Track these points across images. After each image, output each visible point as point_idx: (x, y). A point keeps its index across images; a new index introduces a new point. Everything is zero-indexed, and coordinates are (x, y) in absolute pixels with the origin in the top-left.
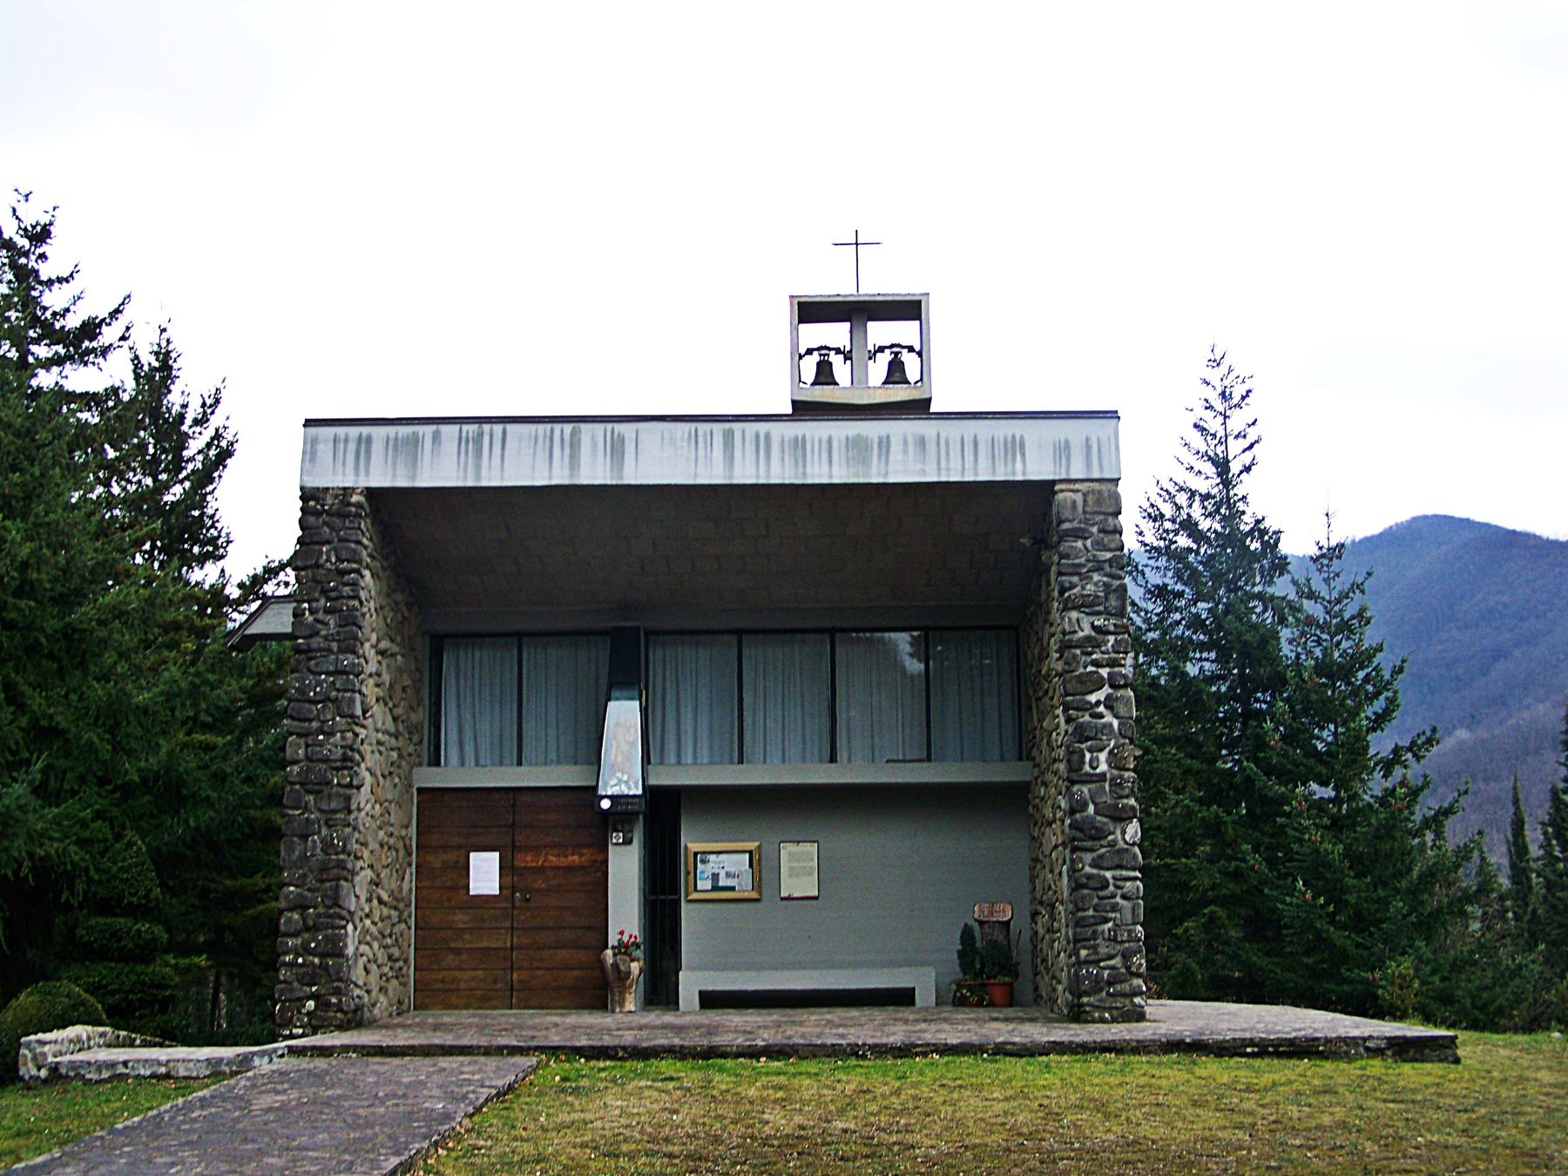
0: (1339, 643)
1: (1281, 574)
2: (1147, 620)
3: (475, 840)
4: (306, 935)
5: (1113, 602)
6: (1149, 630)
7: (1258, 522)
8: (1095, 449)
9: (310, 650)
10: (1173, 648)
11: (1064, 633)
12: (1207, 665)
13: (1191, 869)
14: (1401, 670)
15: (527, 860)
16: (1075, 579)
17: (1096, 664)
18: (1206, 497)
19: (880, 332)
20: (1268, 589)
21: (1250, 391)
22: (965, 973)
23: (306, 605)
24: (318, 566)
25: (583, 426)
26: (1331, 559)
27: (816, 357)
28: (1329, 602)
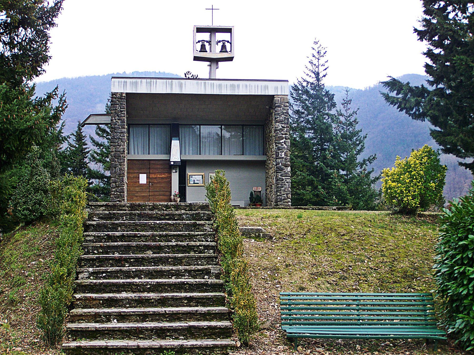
0: (349, 129)
1: (334, 107)
2: (293, 121)
3: (140, 171)
4: (116, 188)
5: (286, 121)
6: (294, 123)
7: (327, 92)
8: (283, 88)
9: (115, 128)
10: (301, 129)
11: (276, 128)
12: (311, 134)
13: (304, 194)
14: (366, 137)
15: (152, 176)
16: (278, 116)
17: (282, 134)
18: (312, 83)
19: (220, 36)
20: (330, 112)
21: (326, 51)
22: (251, 202)
23: (114, 118)
24: (116, 110)
25: (173, 80)
26: (347, 104)
27: (201, 43)
28: (346, 117)
